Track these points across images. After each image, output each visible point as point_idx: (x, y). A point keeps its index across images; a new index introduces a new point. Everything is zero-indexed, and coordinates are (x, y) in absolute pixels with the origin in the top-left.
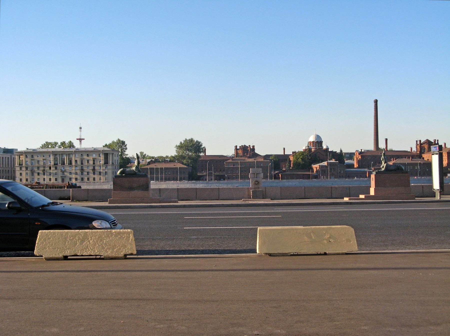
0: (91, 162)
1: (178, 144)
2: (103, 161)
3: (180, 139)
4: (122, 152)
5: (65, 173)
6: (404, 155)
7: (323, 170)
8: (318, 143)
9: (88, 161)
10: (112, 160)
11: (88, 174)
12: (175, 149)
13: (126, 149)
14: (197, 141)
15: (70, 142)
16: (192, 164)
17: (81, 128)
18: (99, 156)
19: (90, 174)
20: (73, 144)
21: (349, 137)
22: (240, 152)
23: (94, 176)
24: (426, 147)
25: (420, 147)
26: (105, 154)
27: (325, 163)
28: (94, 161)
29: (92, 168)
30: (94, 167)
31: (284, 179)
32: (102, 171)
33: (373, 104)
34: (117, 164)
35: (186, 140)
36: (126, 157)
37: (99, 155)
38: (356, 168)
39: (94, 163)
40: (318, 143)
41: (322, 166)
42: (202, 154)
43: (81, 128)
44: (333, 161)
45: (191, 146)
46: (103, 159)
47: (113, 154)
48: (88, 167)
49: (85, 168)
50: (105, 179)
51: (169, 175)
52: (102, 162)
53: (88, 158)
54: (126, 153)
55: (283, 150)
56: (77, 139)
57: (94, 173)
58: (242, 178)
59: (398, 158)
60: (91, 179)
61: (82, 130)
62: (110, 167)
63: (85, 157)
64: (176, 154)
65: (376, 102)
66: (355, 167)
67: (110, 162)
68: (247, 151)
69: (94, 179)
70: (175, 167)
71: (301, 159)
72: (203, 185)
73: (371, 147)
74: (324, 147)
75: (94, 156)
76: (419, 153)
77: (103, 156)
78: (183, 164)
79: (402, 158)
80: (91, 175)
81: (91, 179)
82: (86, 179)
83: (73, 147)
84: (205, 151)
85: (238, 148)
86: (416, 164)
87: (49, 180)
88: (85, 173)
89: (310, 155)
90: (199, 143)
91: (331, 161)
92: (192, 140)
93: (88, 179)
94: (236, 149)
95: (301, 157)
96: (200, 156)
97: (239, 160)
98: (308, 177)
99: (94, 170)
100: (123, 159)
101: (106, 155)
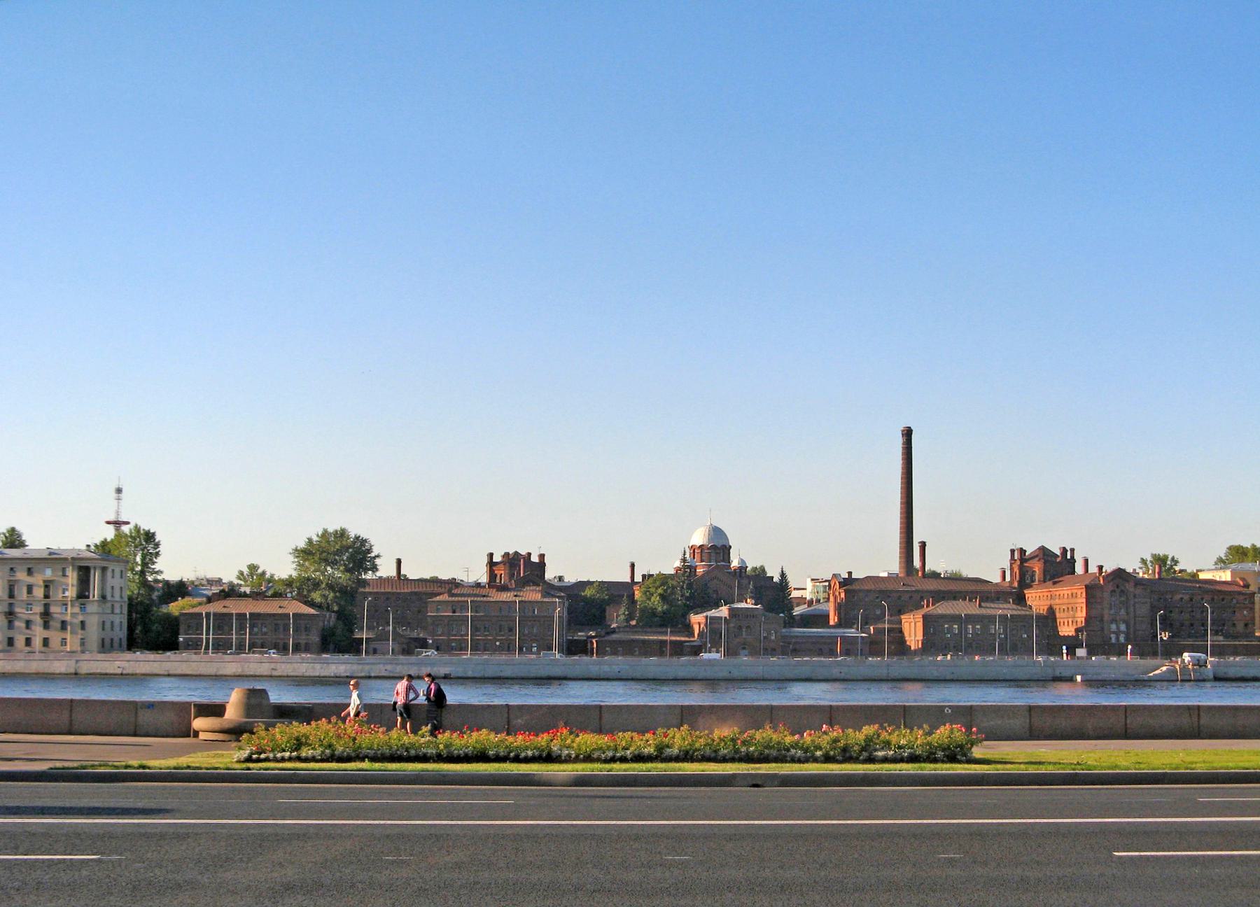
0: (39, 592)
1: (302, 544)
2: (75, 589)
3: (308, 530)
4: (145, 564)
5: (1066, 630)
6: (960, 592)
7: (714, 632)
8: (718, 549)
9: (30, 589)
10: (103, 588)
11: (28, 627)
12: (291, 558)
13: (157, 554)
14: (357, 538)
15: (13, 530)
16: (338, 604)
17: (119, 491)
18: (64, 575)
19: (33, 627)
20: (19, 536)
21: (817, 537)
22: (501, 572)
23: (46, 634)
24: (1036, 569)
25: (1021, 567)
26: (80, 568)
27: (723, 612)
28: (47, 587)
29: (38, 609)
30: (47, 606)
31: (605, 654)
32: (68, 618)
33: (899, 441)
34: (117, 598)
35: (325, 531)
36: (156, 581)
37: (64, 570)
38: (833, 627)
39: (46, 596)
40: (718, 549)
41: (712, 618)
42: (369, 576)
43: (119, 491)
44: (749, 604)
45: (339, 553)
46: (75, 582)
47: (104, 569)
48: (29, 605)
49: (17, 610)
50: (78, 642)
51: (265, 634)
52: (71, 593)
53: (30, 580)
54: (157, 567)
55: (629, 570)
56: (108, 523)
57: (46, 626)
58: (475, 648)
59: (943, 599)
60: (37, 642)
61: (123, 495)
62: (92, 608)
63: (21, 575)
64: (294, 574)
65: (908, 433)
66: (832, 623)
67: (95, 592)
68: (521, 570)
69: (46, 642)
70: (280, 611)
71: (661, 595)
72: (349, 666)
73: (883, 562)
74: (735, 563)
75: (48, 573)
76: (1016, 585)
77: (75, 574)
78: (312, 604)
79: (955, 598)
80: (38, 633)
81: (37, 642)
82: (20, 641)
83: (22, 544)
84: (374, 568)
85: (497, 558)
86: (991, 619)
87: (6, 643)
88: (19, 624)
89: (690, 586)
90: (364, 541)
91: (743, 605)
92: (342, 534)
93: (28, 642)
94: (491, 564)
95: (660, 591)
96: (365, 583)
97: (469, 595)
98: (678, 649)
99: (46, 615)
100: (144, 583)
101: (84, 573)
